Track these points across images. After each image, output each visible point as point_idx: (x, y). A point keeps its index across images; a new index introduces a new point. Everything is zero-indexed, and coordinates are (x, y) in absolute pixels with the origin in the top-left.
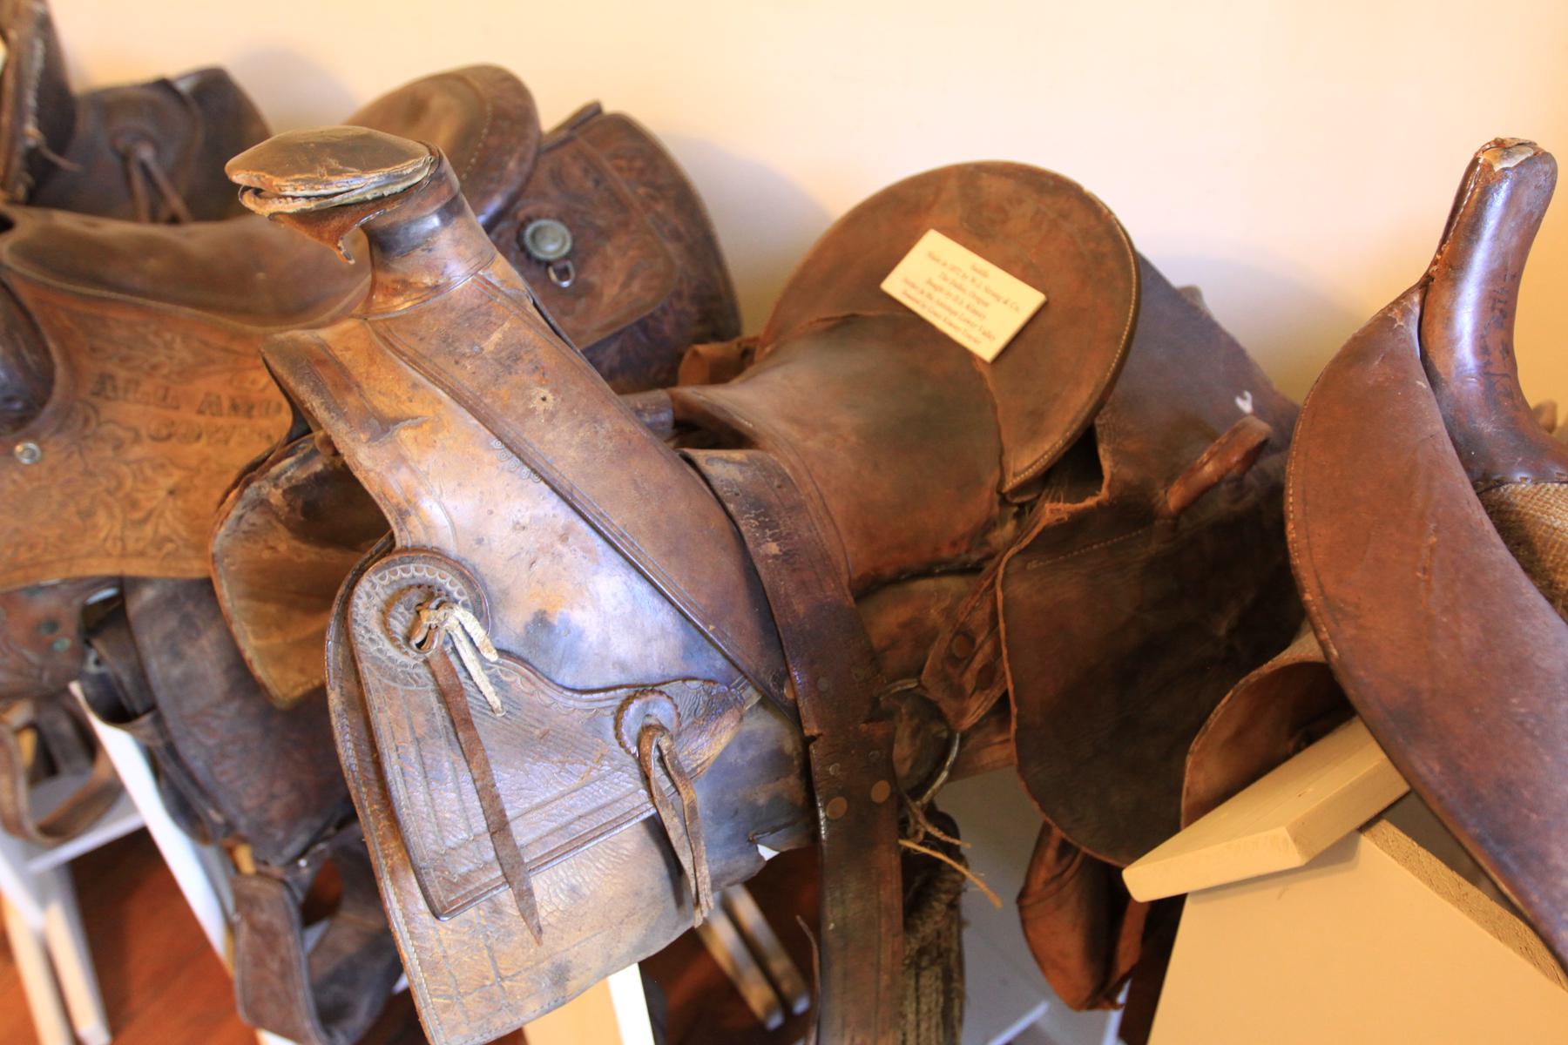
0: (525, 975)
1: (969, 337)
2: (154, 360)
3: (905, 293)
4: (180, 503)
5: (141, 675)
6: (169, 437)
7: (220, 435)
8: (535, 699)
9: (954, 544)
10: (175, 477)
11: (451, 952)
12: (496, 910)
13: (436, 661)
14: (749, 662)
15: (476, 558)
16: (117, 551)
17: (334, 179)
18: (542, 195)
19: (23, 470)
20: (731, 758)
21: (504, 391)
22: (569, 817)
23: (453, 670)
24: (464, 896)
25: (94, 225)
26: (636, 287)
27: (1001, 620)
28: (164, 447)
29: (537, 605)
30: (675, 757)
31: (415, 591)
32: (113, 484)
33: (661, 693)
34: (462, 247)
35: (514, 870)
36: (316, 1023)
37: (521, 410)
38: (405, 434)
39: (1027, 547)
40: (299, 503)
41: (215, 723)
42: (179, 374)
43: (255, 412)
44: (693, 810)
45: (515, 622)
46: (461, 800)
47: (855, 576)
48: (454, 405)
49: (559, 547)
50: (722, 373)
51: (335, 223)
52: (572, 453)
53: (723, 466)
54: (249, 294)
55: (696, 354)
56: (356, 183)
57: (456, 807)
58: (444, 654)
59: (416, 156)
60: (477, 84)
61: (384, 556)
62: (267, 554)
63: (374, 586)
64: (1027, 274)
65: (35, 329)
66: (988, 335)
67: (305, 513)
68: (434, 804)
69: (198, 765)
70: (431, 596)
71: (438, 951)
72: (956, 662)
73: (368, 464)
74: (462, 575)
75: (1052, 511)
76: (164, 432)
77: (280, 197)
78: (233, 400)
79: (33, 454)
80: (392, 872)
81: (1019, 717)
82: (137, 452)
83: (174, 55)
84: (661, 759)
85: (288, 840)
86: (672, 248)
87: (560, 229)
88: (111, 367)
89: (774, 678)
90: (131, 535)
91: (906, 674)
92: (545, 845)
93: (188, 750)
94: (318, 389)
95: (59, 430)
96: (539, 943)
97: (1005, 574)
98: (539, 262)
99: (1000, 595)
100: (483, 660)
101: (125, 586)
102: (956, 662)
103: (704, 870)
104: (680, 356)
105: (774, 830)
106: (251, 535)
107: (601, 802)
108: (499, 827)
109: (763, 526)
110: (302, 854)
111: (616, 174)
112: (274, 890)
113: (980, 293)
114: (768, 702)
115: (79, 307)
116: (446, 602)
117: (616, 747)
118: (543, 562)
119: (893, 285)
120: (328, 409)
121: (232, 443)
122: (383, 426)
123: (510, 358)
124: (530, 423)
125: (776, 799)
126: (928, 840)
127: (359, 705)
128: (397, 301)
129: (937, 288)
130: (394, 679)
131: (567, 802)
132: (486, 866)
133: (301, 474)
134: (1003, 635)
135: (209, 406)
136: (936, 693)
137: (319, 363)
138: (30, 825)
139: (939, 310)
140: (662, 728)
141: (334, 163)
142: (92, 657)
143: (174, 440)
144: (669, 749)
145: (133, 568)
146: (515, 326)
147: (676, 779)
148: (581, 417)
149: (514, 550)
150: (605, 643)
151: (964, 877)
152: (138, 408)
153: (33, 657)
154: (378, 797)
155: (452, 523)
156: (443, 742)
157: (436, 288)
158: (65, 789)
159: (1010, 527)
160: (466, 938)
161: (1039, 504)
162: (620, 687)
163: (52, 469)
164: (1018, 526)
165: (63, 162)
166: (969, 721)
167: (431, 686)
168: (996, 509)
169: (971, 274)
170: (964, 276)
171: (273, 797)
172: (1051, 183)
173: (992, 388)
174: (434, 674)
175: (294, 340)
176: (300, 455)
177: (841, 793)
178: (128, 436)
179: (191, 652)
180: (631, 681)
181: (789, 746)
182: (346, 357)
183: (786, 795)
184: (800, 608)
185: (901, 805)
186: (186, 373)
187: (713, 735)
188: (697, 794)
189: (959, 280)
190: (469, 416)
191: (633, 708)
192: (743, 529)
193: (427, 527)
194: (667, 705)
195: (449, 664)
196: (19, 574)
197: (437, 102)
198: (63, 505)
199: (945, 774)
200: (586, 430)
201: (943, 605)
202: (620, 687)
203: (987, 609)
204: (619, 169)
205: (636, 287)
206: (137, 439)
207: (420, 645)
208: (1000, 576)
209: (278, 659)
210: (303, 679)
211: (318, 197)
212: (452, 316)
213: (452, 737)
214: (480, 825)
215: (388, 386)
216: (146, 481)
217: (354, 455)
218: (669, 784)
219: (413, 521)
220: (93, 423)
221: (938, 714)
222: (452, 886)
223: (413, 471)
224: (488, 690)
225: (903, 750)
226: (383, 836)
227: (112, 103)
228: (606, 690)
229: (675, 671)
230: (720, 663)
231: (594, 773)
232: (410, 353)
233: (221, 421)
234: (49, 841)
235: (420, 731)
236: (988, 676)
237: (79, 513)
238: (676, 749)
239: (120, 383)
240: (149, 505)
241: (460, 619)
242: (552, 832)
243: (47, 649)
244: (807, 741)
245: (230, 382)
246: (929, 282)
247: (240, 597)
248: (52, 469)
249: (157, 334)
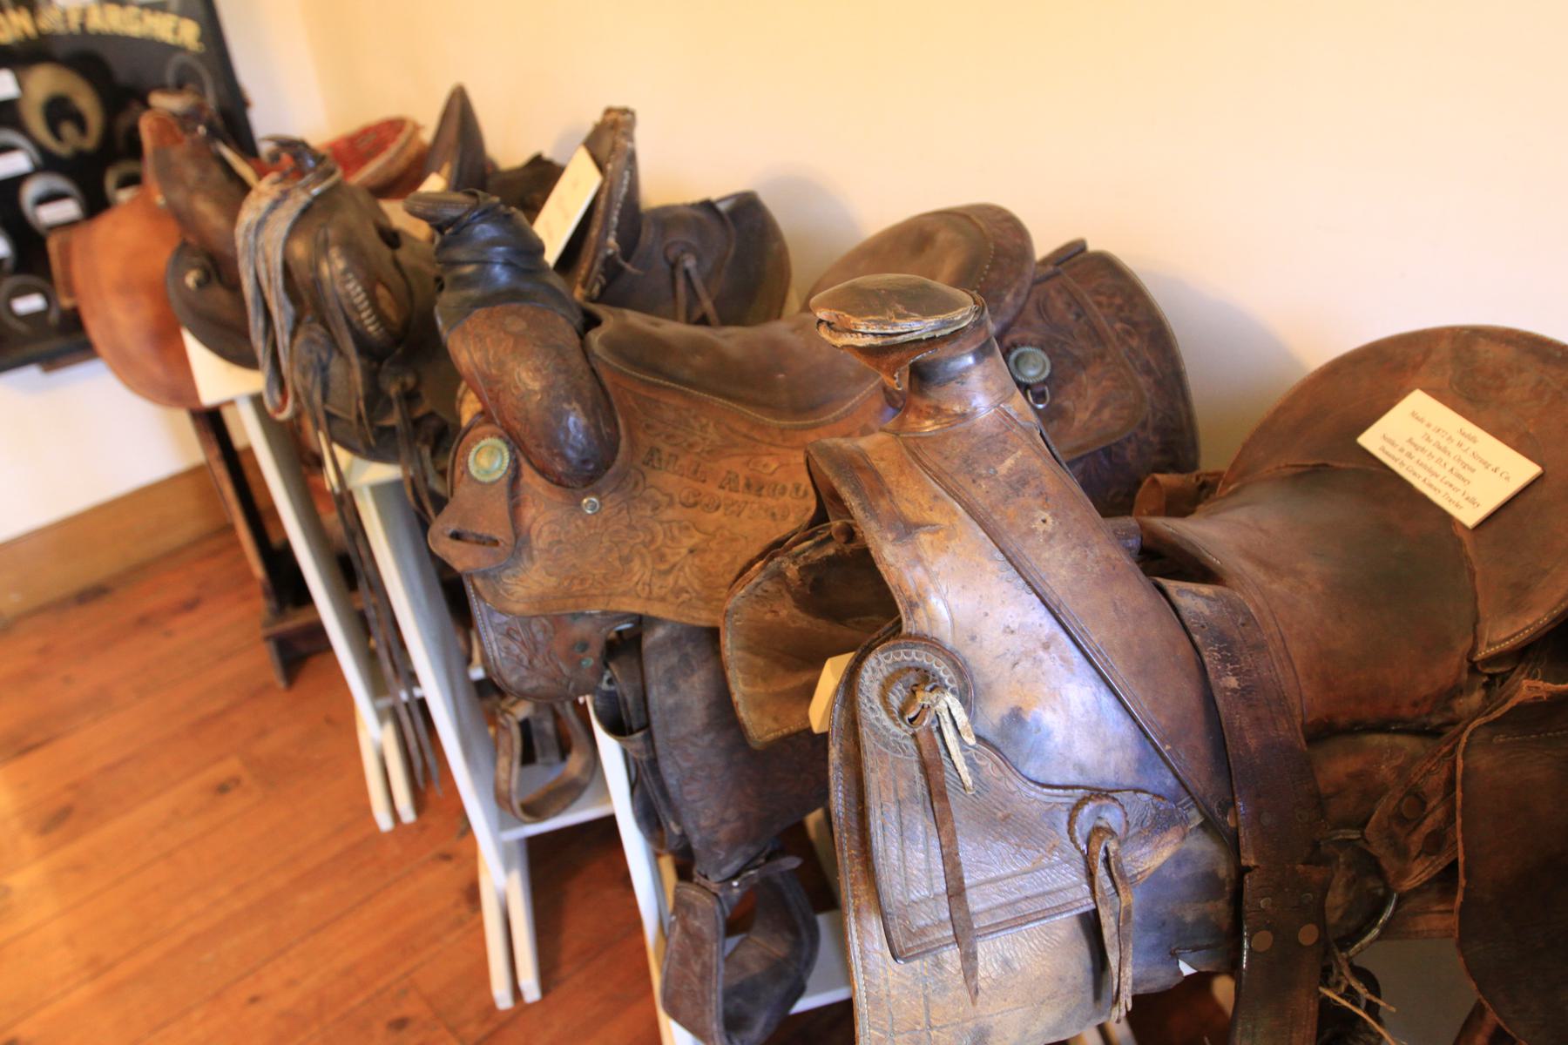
0: (951, 1029)
1: (1430, 485)
2: (691, 440)
3: (1383, 449)
4: (697, 561)
5: (644, 698)
6: (695, 504)
7: (735, 508)
8: (1002, 784)
9: (1415, 704)
10: (696, 539)
11: (894, 992)
12: (938, 965)
13: (923, 737)
14: (1199, 784)
15: (967, 652)
16: (644, 595)
17: (900, 322)
18: (1028, 324)
19: (586, 518)
20: (1166, 873)
21: (1011, 510)
22: (1018, 895)
23: (936, 746)
24: (919, 946)
25: (656, 325)
27: (1459, 788)
28: (690, 513)
29: (1013, 701)
30: (1119, 861)
31: (913, 673)
32: (649, 538)
33: (1115, 799)
34: (989, 384)
35: (964, 933)
36: (722, 1028)
37: (1024, 529)
38: (924, 538)
39: (1496, 720)
40: (810, 579)
41: (691, 750)
42: (709, 452)
43: (764, 492)
44: (1128, 913)
45: (994, 713)
46: (927, 861)
47: (1309, 720)
48: (966, 517)
49: (1041, 653)
50: (1181, 505)
51: (894, 357)
52: (1063, 572)
53: (1192, 598)
54: (780, 393)
55: (1155, 482)
56: (916, 326)
57: (923, 867)
58: (930, 731)
59: (964, 305)
60: (983, 225)
61: (888, 639)
62: (769, 617)
63: (879, 663)
64: (1522, 445)
65: (610, 407)
66: (1473, 501)
67: (812, 588)
68: (907, 858)
69: (671, 782)
70: (926, 680)
71: (884, 989)
72: (1407, 819)
73: (890, 559)
74: (955, 665)
75: (1529, 688)
76: (692, 500)
77: (851, 332)
78: (747, 479)
79: (593, 507)
80: (858, 911)
81: (1466, 890)
82: (669, 514)
83: (715, 181)
84: (1107, 860)
85: (726, 862)
86: (1142, 380)
87: (1042, 356)
88: (659, 443)
89: (1220, 805)
90: (657, 582)
91: (1346, 824)
92: (993, 916)
93: (669, 769)
94: (857, 491)
95: (615, 490)
96: (974, 1003)
97: (1468, 744)
99: (1460, 763)
100: (961, 741)
101: (642, 622)
102: (1407, 819)
103: (1128, 972)
104: (1139, 483)
105: (1196, 949)
106: (762, 599)
107: (1047, 888)
108: (956, 892)
109: (1224, 660)
110: (735, 877)
111: (1095, 308)
112: (708, 901)
113: (1467, 459)
114: (1209, 826)
115: (642, 391)
116: (939, 687)
117: (1068, 841)
118: (1025, 664)
119: (1370, 440)
120: (864, 509)
121: (744, 515)
122: (907, 529)
123: (1019, 482)
124: (1030, 542)
125: (1202, 921)
126: (1350, 994)
127: (855, 762)
128: (928, 423)
129: (1417, 448)
130: (886, 745)
131: (1018, 882)
132: (940, 924)
133: (817, 556)
134: (1459, 803)
135: (729, 482)
136: (1379, 849)
137: (855, 466)
138: (516, 803)
139: (1420, 471)
140: (1112, 833)
141: (900, 308)
142: (606, 678)
144: (1115, 852)
145: (655, 610)
146: (1024, 456)
147: (1118, 881)
148: (1075, 540)
149: (1001, 650)
150: (1069, 745)
151: (1381, 1037)
152: (675, 478)
153: (566, 670)
154: (856, 844)
155: (952, 620)
156: (919, 808)
157: (964, 416)
158: (545, 775)
159: (1477, 697)
160: (908, 983)
161: (1513, 677)
162: (1078, 787)
163: (606, 520)
164: (1487, 696)
165: (628, 266)
166: (1408, 884)
167: (915, 758)
168: (1465, 676)
169: (1458, 438)
170: (1450, 439)
171: (723, 821)
172: (1559, 354)
173: (1471, 553)
174: (919, 747)
175: (839, 447)
176: (818, 538)
177: (1269, 927)
178: (665, 499)
179: (684, 686)
180: (1088, 783)
181: (1223, 871)
182: (881, 466)
183: (1213, 918)
184: (1253, 743)
185: (1327, 953)
186: (714, 453)
187: (1157, 847)
188: (1130, 898)
189: (1444, 443)
190: (978, 528)
191: (1087, 809)
192: (1206, 660)
193: (931, 620)
194: (1118, 812)
195: (933, 740)
196: (571, 601)
197: (943, 237)
198: (610, 550)
199: (1376, 932)
200: (1076, 550)
201: (1395, 763)
202: (1078, 787)
203: (1443, 775)
204: (1099, 304)
205: (1106, 414)
206: (671, 504)
207: (911, 721)
208: (1462, 745)
209: (758, 705)
210: (775, 726)
211: (883, 335)
212: (974, 441)
213: (928, 805)
214: (941, 887)
215: (914, 495)
216: (673, 539)
217: (880, 550)
218: (1110, 885)
219: (920, 613)
220: (641, 485)
221: (1379, 873)
222: (910, 934)
223: (926, 570)
224: (963, 769)
225: (1336, 899)
226: (856, 879)
227: (668, 218)
228: (1065, 787)
229: (1128, 782)
230: (1170, 781)
231: (1045, 861)
232: (934, 468)
233: (736, 496)
234: (527, 818)
235: (902, 795)
236: (1436, 842)
237: (620, 558)
238: (1121, 853)
239: (665, 457)
240: (673, 560)
241: (949, 702)
242: (1001, 906)
243: (577, 664)
244: (1241, 871)
245: (747, 464)
246: (1410, 441)
247: (738, 649)
249: (695, 417)
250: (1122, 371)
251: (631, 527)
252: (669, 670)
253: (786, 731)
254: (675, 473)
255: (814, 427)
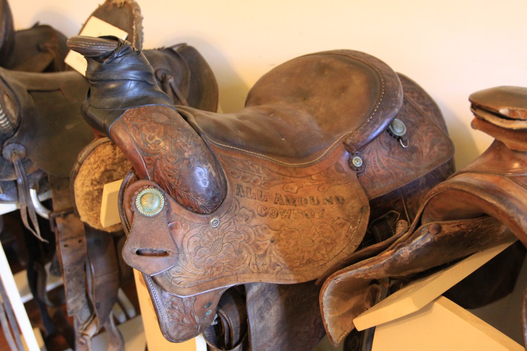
2: (254, 178)
6: (266, 215)
7: (285, 214)
26: (436, 149)
43: (297, 203)
76: (264, 213)
82: (254, 222)
88: (240, 181)
90: (260, 262)
98: (395, 137)
121: (292, 216)
143: (268, 216)
163: (223, 230)
179: (267, 316)
205: (436, 149)
206: (254, 216)
220: (238, 209)
233: (284, 207)
239: (245, 190)
248: (223, 230)
249: (252, 165)
250: (435, 128)
251: (237, 232)
252: (260, 309)
253: (346, 333)
254: (252, 198)
255: (310, 165)
